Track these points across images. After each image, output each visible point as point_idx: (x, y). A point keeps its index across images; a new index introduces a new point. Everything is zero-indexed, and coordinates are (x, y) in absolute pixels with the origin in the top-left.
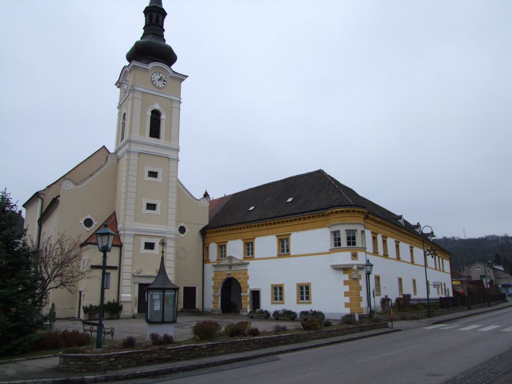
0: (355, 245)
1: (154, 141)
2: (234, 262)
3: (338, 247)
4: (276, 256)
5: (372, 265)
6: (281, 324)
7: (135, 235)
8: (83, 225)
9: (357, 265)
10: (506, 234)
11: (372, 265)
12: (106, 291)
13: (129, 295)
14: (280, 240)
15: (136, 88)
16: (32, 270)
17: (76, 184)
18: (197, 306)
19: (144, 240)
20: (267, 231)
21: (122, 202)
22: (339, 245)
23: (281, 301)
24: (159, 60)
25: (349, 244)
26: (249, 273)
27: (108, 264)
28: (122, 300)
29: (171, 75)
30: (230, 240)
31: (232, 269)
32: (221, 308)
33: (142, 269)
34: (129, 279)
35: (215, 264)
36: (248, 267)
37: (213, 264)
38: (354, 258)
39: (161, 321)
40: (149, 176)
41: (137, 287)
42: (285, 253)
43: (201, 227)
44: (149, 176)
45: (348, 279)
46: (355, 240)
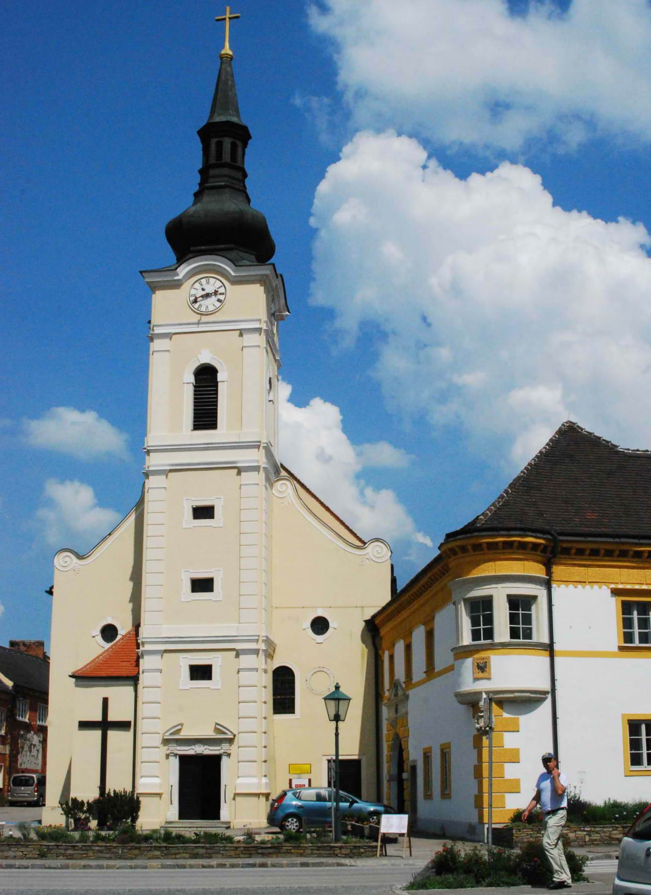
0: (530, 638)
1: (205, 436)
3: (482, 642)
4: (424, 675)
5: (349, 699)
6: (138, 845)
9: (487, 693)
11: (349, 699)
12: (476, 792)
13: (156, 781)
14: (627, 608)
16: (14, 732)
21: (587, 529)
22: (489, 634)
25: (514, 633)
27: (112, 717)
28: (139, 790)
33: (182, 725)
34: (487, 747)
38: (481, 675)
41: (175, 763)
42: (637, 643)
45: (507, 736)
46: (530, 623)
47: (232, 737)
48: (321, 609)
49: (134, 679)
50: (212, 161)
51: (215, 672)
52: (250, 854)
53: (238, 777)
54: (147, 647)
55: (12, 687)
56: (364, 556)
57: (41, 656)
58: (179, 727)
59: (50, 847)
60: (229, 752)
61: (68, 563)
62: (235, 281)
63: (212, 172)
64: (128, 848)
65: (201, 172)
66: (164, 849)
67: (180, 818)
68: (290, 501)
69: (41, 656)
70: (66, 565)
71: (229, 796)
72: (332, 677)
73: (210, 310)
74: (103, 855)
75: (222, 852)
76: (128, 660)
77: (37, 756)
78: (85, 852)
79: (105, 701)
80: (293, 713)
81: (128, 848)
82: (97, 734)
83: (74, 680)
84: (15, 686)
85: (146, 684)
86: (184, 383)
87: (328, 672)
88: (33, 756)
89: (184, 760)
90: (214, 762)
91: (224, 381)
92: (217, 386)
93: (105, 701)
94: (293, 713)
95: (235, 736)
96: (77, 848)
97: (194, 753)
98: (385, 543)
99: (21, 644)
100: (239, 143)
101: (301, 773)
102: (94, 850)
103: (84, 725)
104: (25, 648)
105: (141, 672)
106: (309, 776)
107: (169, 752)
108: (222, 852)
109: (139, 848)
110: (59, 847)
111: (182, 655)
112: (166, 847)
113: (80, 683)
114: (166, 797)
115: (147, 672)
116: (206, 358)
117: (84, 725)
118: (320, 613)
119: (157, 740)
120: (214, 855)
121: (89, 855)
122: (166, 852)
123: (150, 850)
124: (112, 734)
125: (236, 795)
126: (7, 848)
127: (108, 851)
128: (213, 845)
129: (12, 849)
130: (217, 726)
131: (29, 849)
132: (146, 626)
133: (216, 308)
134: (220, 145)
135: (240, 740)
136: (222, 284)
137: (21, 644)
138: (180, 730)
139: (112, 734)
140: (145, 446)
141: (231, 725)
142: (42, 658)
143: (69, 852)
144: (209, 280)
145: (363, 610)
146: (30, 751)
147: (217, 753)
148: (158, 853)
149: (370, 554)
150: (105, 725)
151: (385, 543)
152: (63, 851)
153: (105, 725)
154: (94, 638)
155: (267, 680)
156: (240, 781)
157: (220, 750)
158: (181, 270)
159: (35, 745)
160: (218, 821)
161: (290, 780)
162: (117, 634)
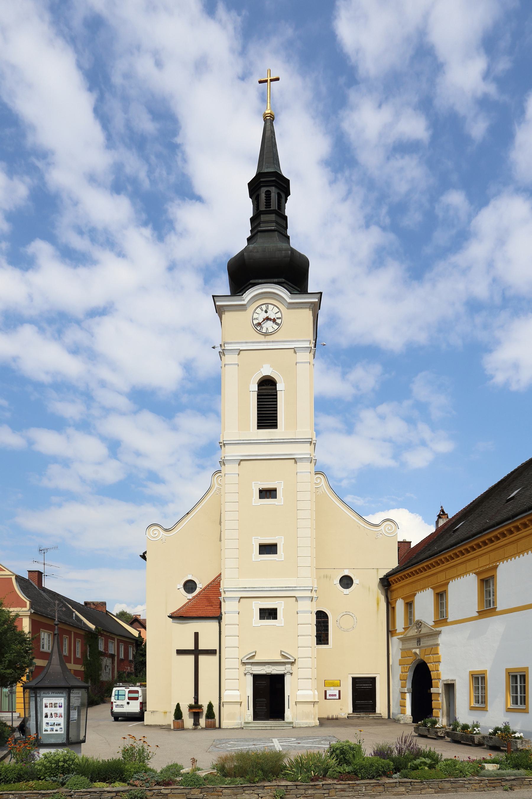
1: (266, 433)
2: (424, 631)
4: (476, 614)
7: (241, 598)
8: (182, 590)
10: (294, 353)
13: (237, 693)
15: (227, 347)
17: (166, 530)
18: (378, 710)
19: (258, 605)
20: (463, 566)
23: (523, 707)
24: (260, 281)
26: (441, 650)
29: (289, 301)
30: (418, 590)
31: (421, 645)
32: (412, 715)
35: (402, 636)
36: (441, 640)
37: (400, 636)
39: (65, 741)
40: (261, 497)
41: (250, 680)
43: (383, 573)
44: (260, 498)
47: (294, 661)
48: (348, 570)
49: (219, 618)
50: (262, 208)
51: (280, 614)
52: (494, 787)
53: (298, 690)
54: (228, 595)
55: (95, 629)
56: (379, 532)
57: (105, 611)
58: (254, 654)
59: (289, 788)
60: (291, 672)
61: (157, 535)
62: (291, 306)
63: (263, 218)
64: (372, 785)
65: (252, 220)
66: (409, 784)
67: (254, 720)
68: (323, 491)
69: (105, 611)
70: (157, 535)
71: (292, 703)
72: (355, 618)
73: (269, 332)
74: (346, 794)
75: (467, 786)
76: (211, 605)
77: (109, 672)
78: (327, 791)
79: (196, 635)
80: (328, 644)
81: (372, 785)
82: (192, 658)
83: (171, 619)
84: (96, 628)
85: (226, 623)
86: (250, 391)
87: (353, 616)
88: (107, 672)
89: (256, 678)
90: (278, 680)
91: (282, 391)
92: (277, 393)
93: (196, 635)
94: (328, 644)
95: (295, 660)
96: (317, 787)
97: (265, 673)
98: (394, 522)
99: (92, 604)
100: (283, 195)
101: (333, 685)
102: (336, 788)
103: (180, 652)
104: (95, 606)
105: (223, 613)
106: (339, 688)
107: (247, 671)
108: (467, 786)
109: (383, 785)
110: (298, 787)
111: (254, 601)
112: (411, 782)
113: (173, 621)
114: (245, 704)
115: (228, 613)
116: (267, 371)
117: (180, 652)
118: (346, 573)
119: (237, 663)
120: (459, 789)
121: (331, 794)
122: (410, 788)
123: (396, 786)
124: (202, 658)
125: (296, 703)
126: (241, 791)
127: (351, 790)
128: (457, 779)
129: (247, 792)
130: (283, 653)
131: (265, 791)
132: (226, 579)
133: (274, 330)
134: (268, 194)
135: (299, 663)
136: (278, 310)
137: (92, 604)
138: (254, 656)
139: (202, 658)
140: (221, 441)
141: (292, 653)
142: (105, 613)
143: (310, 792)
144: (268, 306)
145: (377, 571)
146: (106, 670)
147: (282, 672)
148: (403, 789)
149: (383, 530)
150: (196, 652)
151: (394, 522)
152: (303, 792)
153: (196, 652)
154: (179, 590)
155: (313, 619)
156: (299, 693)
157: (284, 670)
158: (245, 296)
159: (108, 666)
160: (284, 721)
161: (326, 692)
162: (195, 589)
